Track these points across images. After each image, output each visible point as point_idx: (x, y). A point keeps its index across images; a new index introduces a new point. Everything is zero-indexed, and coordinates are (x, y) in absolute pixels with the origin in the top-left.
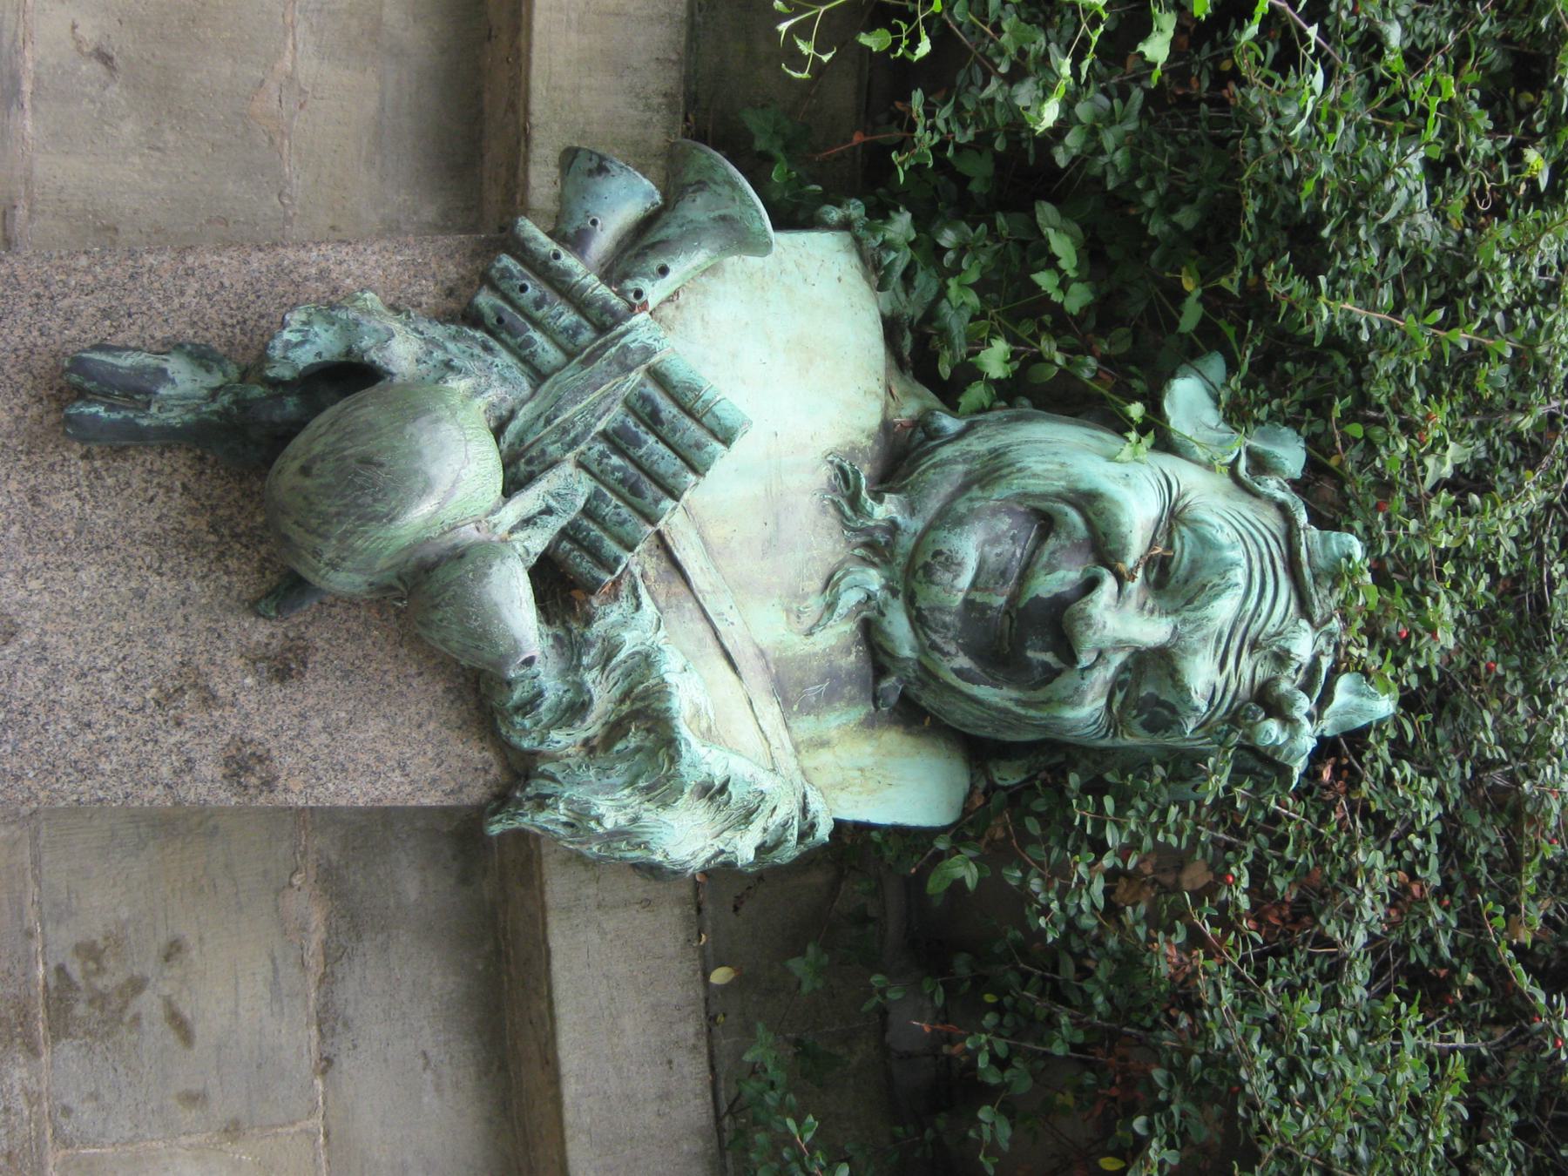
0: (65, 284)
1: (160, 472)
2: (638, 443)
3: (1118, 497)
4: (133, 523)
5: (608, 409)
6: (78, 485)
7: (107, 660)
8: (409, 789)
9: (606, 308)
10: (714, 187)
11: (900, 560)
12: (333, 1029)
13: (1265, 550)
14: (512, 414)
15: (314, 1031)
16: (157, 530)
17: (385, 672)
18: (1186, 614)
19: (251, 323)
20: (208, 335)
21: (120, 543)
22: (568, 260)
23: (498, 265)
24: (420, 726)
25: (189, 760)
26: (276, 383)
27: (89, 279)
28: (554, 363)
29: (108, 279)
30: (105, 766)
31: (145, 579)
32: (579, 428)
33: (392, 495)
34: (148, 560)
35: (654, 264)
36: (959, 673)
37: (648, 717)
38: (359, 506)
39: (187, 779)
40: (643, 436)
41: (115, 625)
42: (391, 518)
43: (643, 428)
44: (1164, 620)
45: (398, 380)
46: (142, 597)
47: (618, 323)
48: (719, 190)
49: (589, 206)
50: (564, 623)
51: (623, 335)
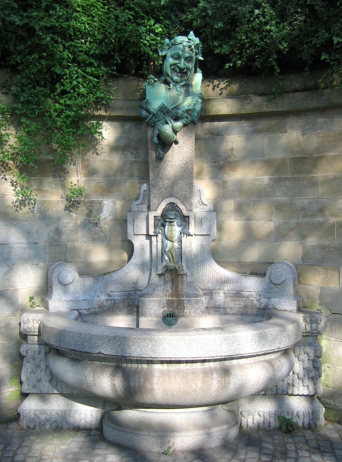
22: (149, 118)
26: (160, 142)
36: (187, 77)
42: (170, 135)
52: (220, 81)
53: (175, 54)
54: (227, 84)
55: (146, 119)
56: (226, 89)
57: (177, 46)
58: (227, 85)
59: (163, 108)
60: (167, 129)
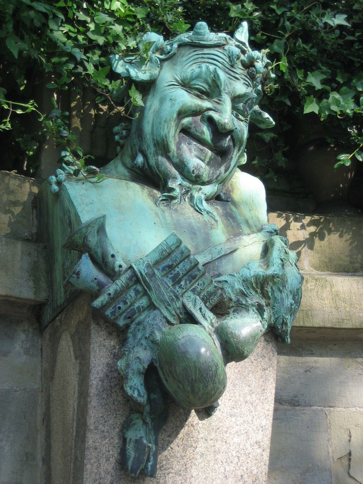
0: (96, 473)
1: (163, 444)
2: (178, 274)
3: (181, 104)
4: (179, 456)
5: (166, 283)
6: (164, 474)
7: (222, 468)
8: (271, 368)
9: (130, 279)
10: (87, 233)
11: (191, 185)
12: (297, 401)
13: (201, 56)
14: (165, 318)
15: (297, 408)
16: (182, 447)
17: (234, 372)
18: (222, 89)
19: (116, 408)
20: (119, 423)
21: (185, 461)
23: (110, 316)
24: (252, 362)
25: (256, 443)
27: (95, 465)
28: (147, 300)
29: (96, 458)
30: (255, 472)
31: (197, 453)
32: (172, 294)
33: (210, 364)
34: (191, 451)
35: (110, 259)
36: (226, 171)
37: (264, 283)
38: (212, 376)
39: (262, 444)
40: (176, 272)
41: (211, 464)
43: (173, 272)
44: (223, 97)
45: (155, 357)
46: (203, 454)
47: (136, 275)
48: (89, 231)
49: (89, 280)
50: (229, 308)
51: (141, 274)
52: (287, 219)
53: (198, 77)
54: (312, 229)
55: (96, 295)
56: (311, 247)
57: (206, 51)
58: (312, 235)
59: (177, 254)
60: (201, 339)
